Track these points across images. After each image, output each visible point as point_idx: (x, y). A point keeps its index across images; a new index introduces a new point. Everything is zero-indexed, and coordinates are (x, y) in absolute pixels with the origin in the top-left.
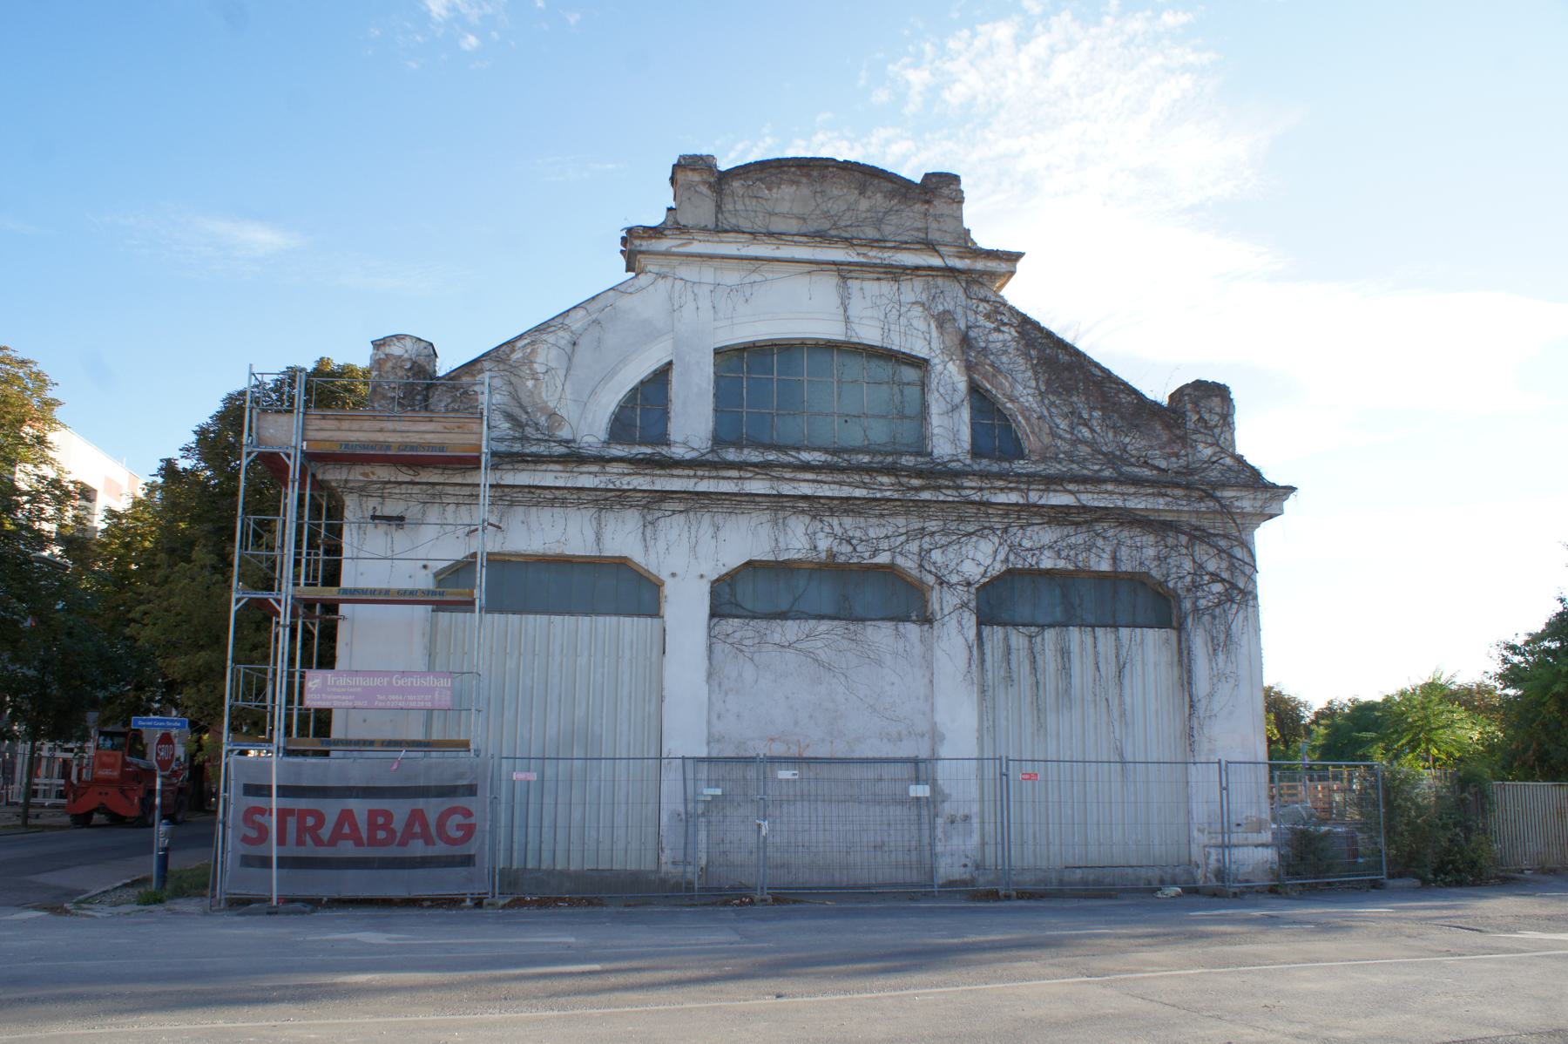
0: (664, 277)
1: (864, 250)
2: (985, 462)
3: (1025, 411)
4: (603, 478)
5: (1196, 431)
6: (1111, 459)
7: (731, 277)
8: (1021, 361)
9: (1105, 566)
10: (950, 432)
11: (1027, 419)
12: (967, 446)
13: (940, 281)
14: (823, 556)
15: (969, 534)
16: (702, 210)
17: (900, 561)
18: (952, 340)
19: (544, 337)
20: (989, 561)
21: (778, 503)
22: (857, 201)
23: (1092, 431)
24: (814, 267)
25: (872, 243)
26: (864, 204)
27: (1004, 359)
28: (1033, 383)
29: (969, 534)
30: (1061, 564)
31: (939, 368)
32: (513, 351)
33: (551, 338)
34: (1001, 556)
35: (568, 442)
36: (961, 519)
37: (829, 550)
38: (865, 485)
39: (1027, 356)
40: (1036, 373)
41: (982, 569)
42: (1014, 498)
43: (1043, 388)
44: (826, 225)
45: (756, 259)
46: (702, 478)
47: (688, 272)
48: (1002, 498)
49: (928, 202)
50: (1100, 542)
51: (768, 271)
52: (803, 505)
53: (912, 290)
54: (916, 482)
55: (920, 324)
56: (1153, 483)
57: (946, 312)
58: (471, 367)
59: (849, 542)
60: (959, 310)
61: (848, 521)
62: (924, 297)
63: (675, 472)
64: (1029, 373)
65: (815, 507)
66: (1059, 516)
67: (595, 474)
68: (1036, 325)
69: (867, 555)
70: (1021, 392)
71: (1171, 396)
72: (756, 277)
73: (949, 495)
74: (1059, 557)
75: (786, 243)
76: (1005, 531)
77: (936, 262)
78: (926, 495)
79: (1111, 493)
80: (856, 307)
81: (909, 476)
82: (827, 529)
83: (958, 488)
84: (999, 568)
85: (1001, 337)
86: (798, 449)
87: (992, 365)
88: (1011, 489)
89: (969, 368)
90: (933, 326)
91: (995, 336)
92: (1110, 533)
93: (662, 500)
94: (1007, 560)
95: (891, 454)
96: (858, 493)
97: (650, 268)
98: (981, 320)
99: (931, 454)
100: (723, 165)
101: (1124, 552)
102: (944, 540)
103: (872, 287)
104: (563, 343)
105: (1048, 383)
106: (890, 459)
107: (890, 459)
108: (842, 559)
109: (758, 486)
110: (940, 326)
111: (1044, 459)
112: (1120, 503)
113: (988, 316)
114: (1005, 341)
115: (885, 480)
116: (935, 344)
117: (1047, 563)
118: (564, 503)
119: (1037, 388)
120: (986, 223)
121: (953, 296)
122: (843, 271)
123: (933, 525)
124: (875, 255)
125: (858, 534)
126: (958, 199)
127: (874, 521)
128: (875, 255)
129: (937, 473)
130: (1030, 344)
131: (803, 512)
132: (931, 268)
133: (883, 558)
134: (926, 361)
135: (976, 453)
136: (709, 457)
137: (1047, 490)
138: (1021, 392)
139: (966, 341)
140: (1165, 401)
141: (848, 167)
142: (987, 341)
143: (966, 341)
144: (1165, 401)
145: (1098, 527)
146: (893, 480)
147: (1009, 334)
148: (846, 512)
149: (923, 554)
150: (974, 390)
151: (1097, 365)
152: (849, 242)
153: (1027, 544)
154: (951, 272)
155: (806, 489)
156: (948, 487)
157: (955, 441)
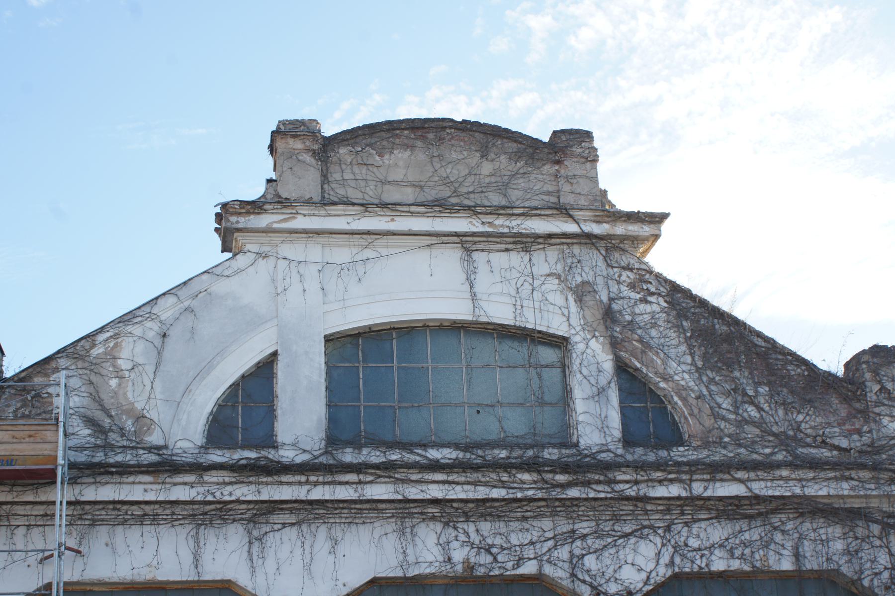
0: (265, 256)
1: (489, 218)
2: (639, 451)
3: (681, 391)
4: (201, 489)
5: (879, 404)
6: (783, 440)
7: (341, 254)
8: (672, 334)
9: (787, 565)
10: (597, 421)
11: (684, 400)
12: (617, 434)
13: (576, 250)
14: (459, 568)
15: (626, 536)
16: (305, 181)
17: (548, 570)
18: (593, 314)
19: (129, 328)
20: (651, 566)
21: (405, 511)
22: (479, 165)
23: (759, 409)
24: (434, 240)
25: (497, 211)
26: (487, 168)
27: (654, 333)
28: (689, 359)
29: (626, 536)
30: (735, 565)
31: (581, 347)
32: (93, 346)
33: (137, 330)
34: (665, 559)
35: (159, 448)
36: (616, 518)
37: (466, 562)
38: (503, 485)
39: (679, 328)
40: (690, 347)
41: (644, 576)
42: (675, 490)
43: (700, 364)
44: (446, 192)
45: (369, 233)
46: (316, 484)
47: (293, 250)
48: (661, 491)
49: (558, 162)
50: (778, 537)
51: (382, 246)
52: (433, 510)
53: (545, 261)
54: (561, 478)
55: (557, 299)
56: (834, 465)
57: (585, 283)
58: (45, 365)
59: (488, 551)
60: (600, 281)
61: (486, 527)
62: (559, 268)
63: (284, 478)
64: (683, 348)
65: (446, 512)
66: (728, 510)
67: (192, 485)
68: (687, 293)
69: (509, 565)
70: (676, 368)
71: (847, 365)
72: (369, 253)
73: (601, 491)
74: (732, 556)
75: (402, 214)
76: (668, 529)
77: (571, 228)
78: (574, 493)
79: (786, 479)
80: (483, 282)
81: (554, 472)
82: (462, 537)
83: (611, 482)
84: (663, 573)
85: (648, 308)
86: (425, 446)
87: (641, 340)
88: (671, 481)
89: (615, 345)
90: (571, 299)
91: (642, 307)
92: (790, 526)
93: (271, 512)
94: (672, 563)
95: (531, 447)
96: (496, 493)
97: (249, 247)
98: (626, 291)
99: (577, 445)
100: (328, 130)
101: (807, 548)
102: (598, 544)
103: (500, 259)
104: (150, 335)
105: (705, 357)
106: (530, 453)
107: (530, 453)
108: (481, 571)
109: (381, 491)
110: (579, 300)
111: (706, 445)
112: (798, 491)
113: (632, 286)
114: (653, 314)
115: (526, 477)
116: (574, 320)
117: (719, 565)
118: (155, 520)
119: (693, 363)
120: (624, 182)
121: (591, 265)
122: (467, 243)
123: (584, 527)
124: (502, 224)
125: (498, 541)
126: (592, 158)
127: (515, 525)
128: (502, 224)
129: (584, 467)
130: (682, 314)
131: (433, 518)
132: (565, 235)
133: (529, 568)
134: (565, 340)
135: (628, 441)
136: (323, 459)
137: (713, 480)
138: (676, 368)
139: (609, 315)
140: (840, 371)
141: (468, 127)
142: (633, 314)
143: (609, 315)
144: (840, 371)
145: (775, 520)
146: (535, 477)
147: (657, 305)
148: (484, 516)
149: (575, 561)
150: (622, 369)
151: (759, 335)
152: (472, 210)
153: (694, 543)
154: (588, 239)
155: (436, 492)
156: (599, 482)
157: (603, 428)
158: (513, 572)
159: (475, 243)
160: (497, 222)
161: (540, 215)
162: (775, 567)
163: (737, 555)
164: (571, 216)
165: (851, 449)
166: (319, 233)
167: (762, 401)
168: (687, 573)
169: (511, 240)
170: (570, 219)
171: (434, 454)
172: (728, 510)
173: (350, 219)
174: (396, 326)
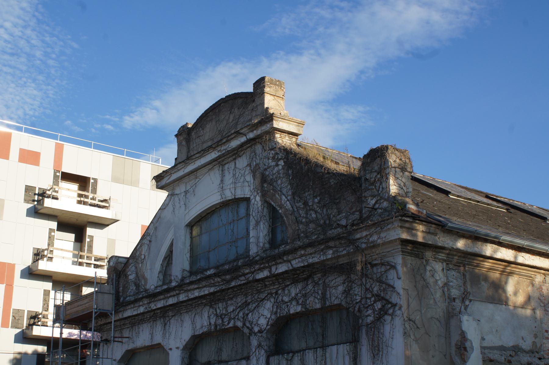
1: (219, 148)
24: (210, 166)
46: (169, 298)
77: (243, 139)
122: (219, 162)
158: (228, 326)
159: (223, 161)
160: (222, 148)
161: (232, 138)
162: (315, 308)
163: (300, 302)
164: (241, 134)
165: (347, 225)
166: (192, 172)
167: (316, 207)
168: (293, 314)
169: (232, 153)
170: (241, 135)
171: (209, 273)
172: (294, 276)
173: (183, 170)
174: (209, 212)
